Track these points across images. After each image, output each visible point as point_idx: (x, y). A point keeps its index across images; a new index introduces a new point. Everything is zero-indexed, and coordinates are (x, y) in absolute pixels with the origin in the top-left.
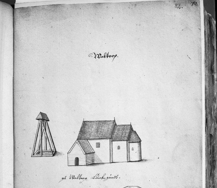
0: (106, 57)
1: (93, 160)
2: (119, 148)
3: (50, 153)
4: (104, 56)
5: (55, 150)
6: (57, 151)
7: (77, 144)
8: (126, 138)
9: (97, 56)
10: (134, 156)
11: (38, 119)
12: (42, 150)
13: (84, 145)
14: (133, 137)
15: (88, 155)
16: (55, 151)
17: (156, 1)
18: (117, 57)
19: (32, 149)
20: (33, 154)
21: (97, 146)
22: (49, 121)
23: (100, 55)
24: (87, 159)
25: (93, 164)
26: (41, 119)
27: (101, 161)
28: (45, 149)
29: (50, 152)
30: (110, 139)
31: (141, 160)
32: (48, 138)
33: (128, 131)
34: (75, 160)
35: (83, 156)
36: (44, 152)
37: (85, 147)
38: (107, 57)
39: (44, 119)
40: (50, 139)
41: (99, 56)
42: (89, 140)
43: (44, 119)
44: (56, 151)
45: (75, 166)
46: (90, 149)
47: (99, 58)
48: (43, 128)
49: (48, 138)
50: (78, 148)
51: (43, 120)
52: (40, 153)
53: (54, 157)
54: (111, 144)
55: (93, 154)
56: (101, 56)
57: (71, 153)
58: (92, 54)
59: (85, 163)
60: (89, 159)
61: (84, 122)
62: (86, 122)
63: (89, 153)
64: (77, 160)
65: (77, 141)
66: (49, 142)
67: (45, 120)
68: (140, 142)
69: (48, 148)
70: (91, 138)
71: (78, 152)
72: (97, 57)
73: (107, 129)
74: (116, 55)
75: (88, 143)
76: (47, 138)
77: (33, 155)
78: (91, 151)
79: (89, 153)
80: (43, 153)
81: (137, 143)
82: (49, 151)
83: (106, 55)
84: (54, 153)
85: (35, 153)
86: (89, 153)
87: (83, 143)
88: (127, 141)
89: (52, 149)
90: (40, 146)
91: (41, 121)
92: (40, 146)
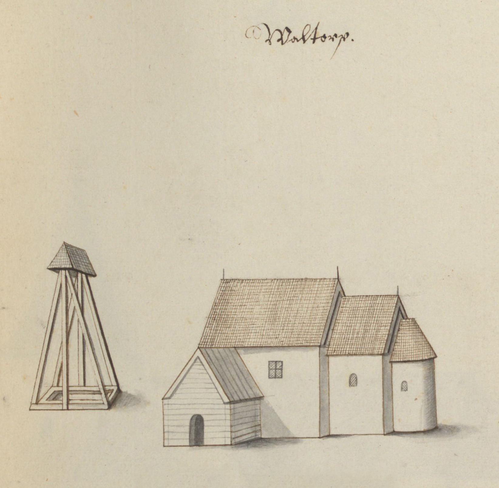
0: (309, 42)
1: (257, 427)
2: (353, 381)
3: (97, 397)
4: (303, 38)
5: (118, 385)
6: (123, 389)
7: (197, 368)
8: (380, 347)
9: (277, 35)
10: (410, 412)
11: (56, 270)
12: (68, 387)
13: (225, 368)
14: (406, 342)
15: (237, 405)
16: (115, 389)
17: (428, 343)
18: (348, 40)
19: (33, 380)
20: (34, 401)
21: (273, 373)
22: (95, 276)
23: (286, 34)
24: (236, 422)
25: (256, 442)
26: (65, 269)
27: (285, 428)
28: (82, 384)
29: (99, 393)
30: (320, 346)
31: (434, 429)
32: (90, 339)
33: (387, 320)
34: (191, 426)
35: (222, 412)
36: (76, 392)
37: (229, 375)
38: (314, 39)
39: (76, 267)
40: (97, 343)
41: (284, 35)
42: (241, 351)
43: (76, 267)
44: (119, 391)
45: (190, 446)
46: (247, 387)
47: (282, 44)
48: (74, 303)
49: (90, 339)
50: (202, 378)
51: (74, 271)
52: (61, 397)
53: (112, 411)
54: (324, 359)
55: (257, 402)
56: (291, 37)
57: (175, 396)
58: (257, 30)
59: (228, 434)
60: (241, 421)
61: (225, 281)
62: (231, 284)
63: (241, 401)
64: (198, 423)
65: (198, 353)
66: (94, 353)
67: (82, 273)
68: (430, 361)
69: (93, 380)
70: (252, 341)
71: (205, 396)
72: (274, 40)
73: (312, 309)
74: (348, 34)
75: (239, 362)
76: (86, 340)
77: (37, 403)
78: (250, 392)
79: (241, 401)
80: (71, 397)
81: (420, 364)
82: (101, 402)
83: (309, 35)
84: (115, 398)
85: (41, 395)
86: (244, 399)
87: (222, 363)
88: (383, 355)
89: (107, 382)
90: (63, 370)
91: (66, 277)
92: (63, 370)
